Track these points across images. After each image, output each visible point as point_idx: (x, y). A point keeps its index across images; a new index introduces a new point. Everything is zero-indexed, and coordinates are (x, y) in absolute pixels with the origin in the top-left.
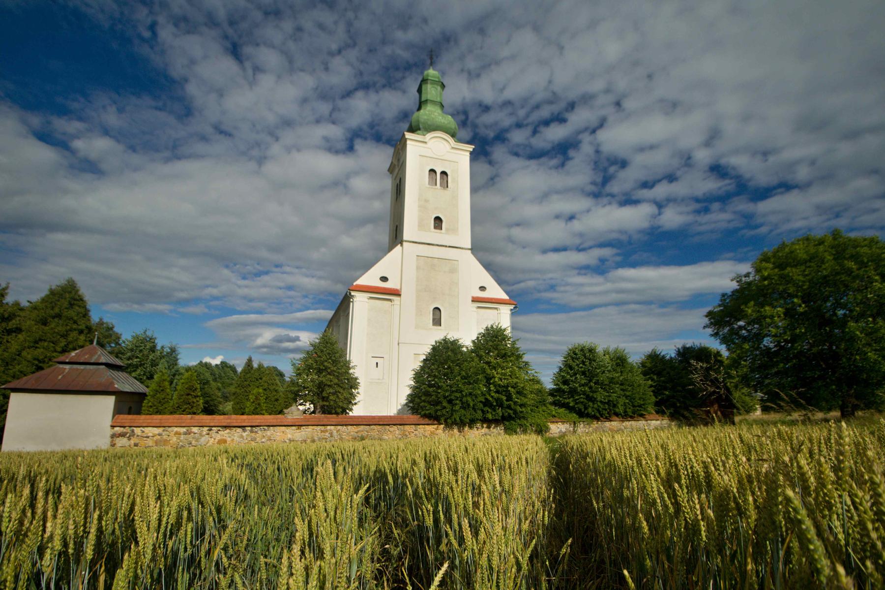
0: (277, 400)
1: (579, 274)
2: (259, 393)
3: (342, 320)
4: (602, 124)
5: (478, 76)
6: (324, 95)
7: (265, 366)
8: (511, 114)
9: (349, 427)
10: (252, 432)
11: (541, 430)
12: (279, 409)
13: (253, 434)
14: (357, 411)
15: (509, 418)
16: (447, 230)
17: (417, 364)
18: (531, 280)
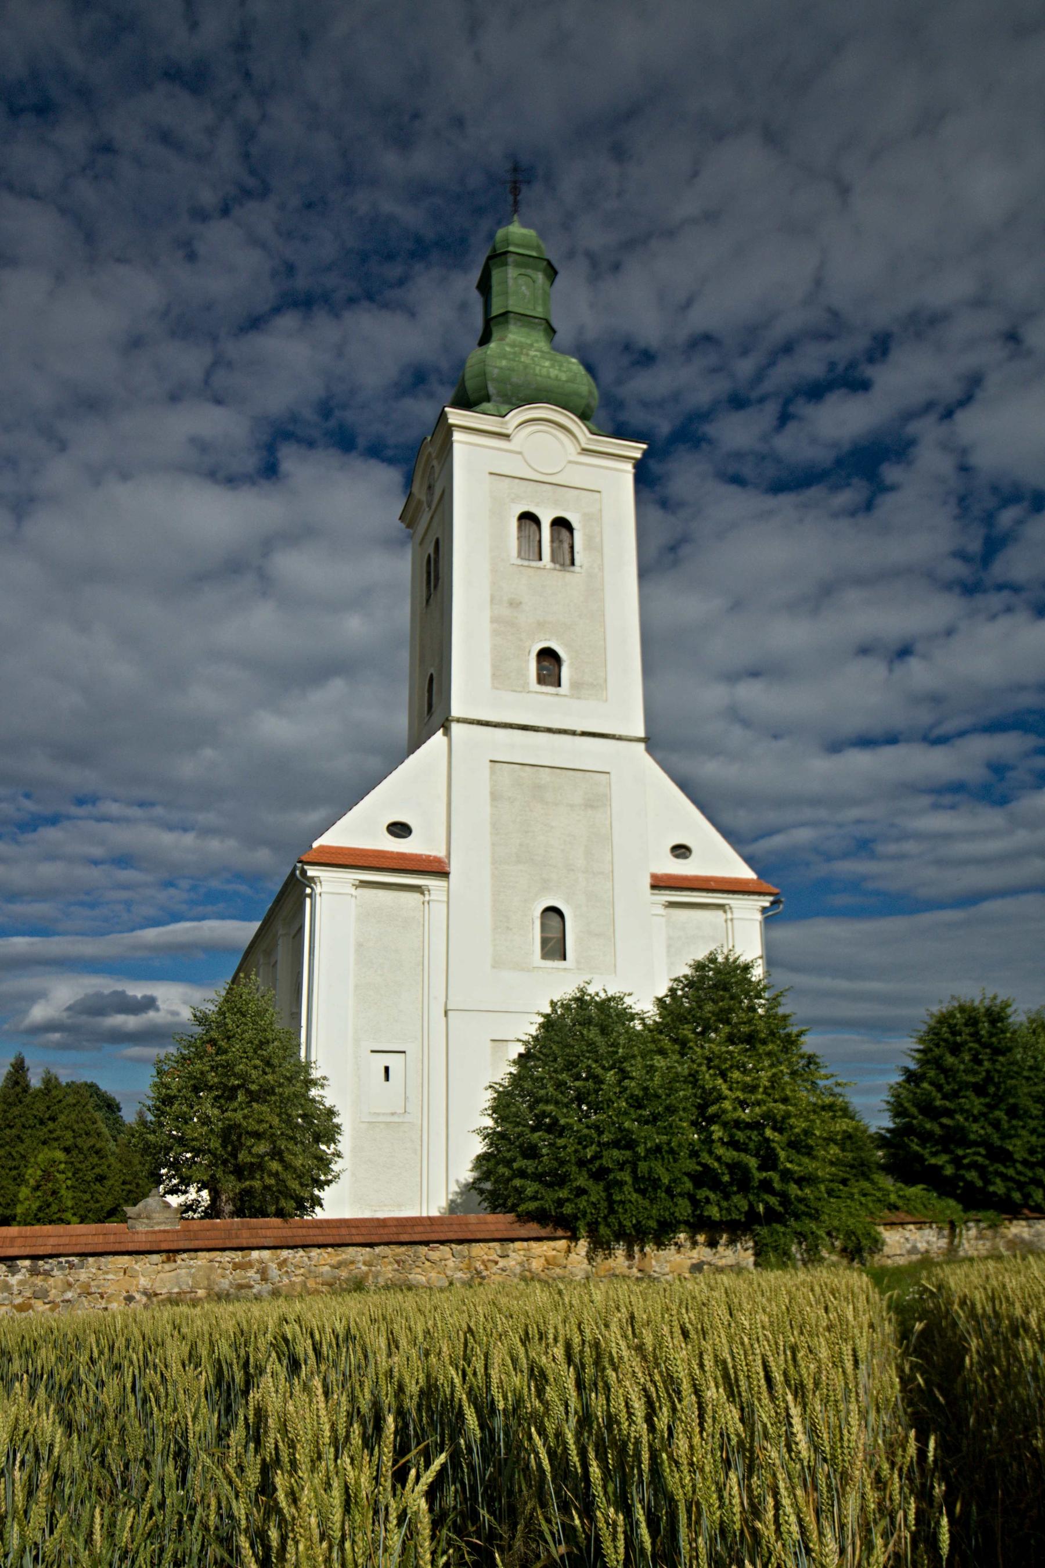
0: (101, 1179)
1: (936, 807)
2: (53, 1162)
3: (282, 953)
4: (971, 389)
5: (616, 267)
6: (184, 324)
7: (64, 1080)
8: (715, 370)
9: (315, 1253)
10: (34, 1272)
11: (858, 1249)
12: (108, 1203)
13: (38, 1281)
14: (336, 1204)
15: (772, 1217)
16: (576, 686)
17: (502, 1070)
18: (803, 825)
